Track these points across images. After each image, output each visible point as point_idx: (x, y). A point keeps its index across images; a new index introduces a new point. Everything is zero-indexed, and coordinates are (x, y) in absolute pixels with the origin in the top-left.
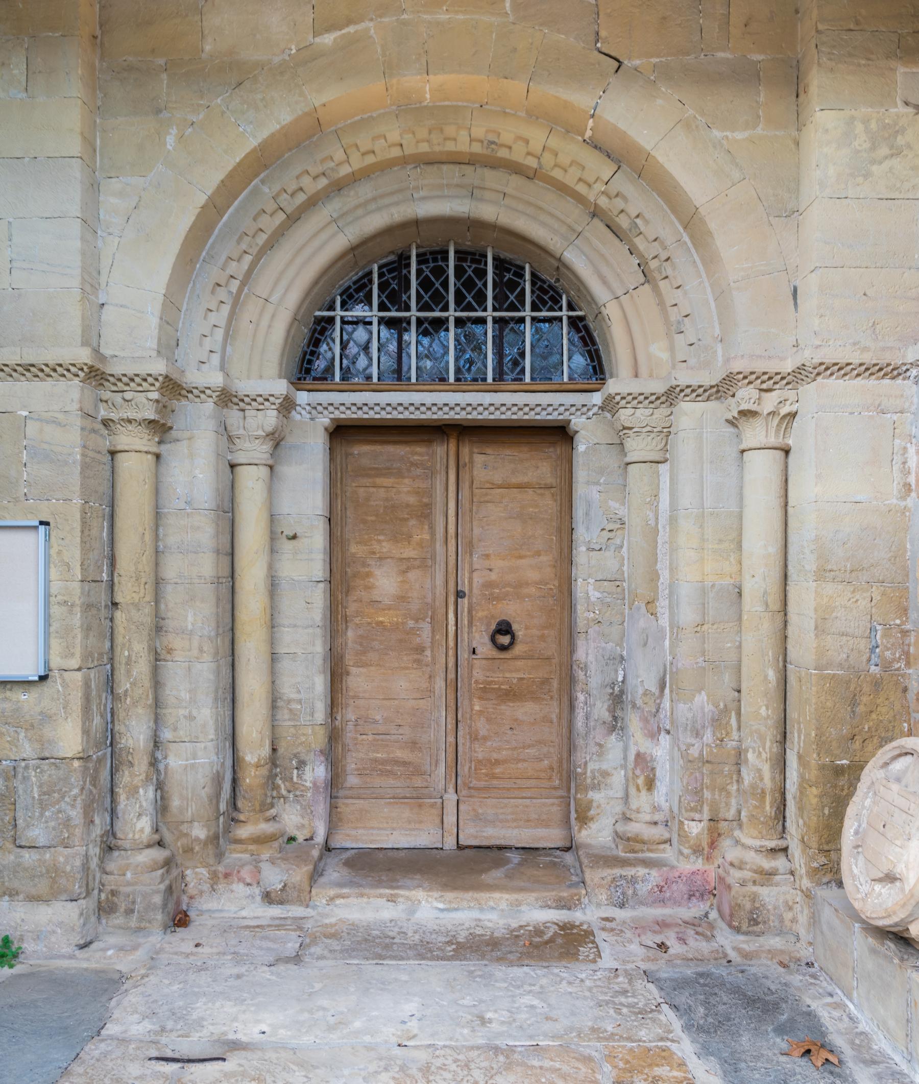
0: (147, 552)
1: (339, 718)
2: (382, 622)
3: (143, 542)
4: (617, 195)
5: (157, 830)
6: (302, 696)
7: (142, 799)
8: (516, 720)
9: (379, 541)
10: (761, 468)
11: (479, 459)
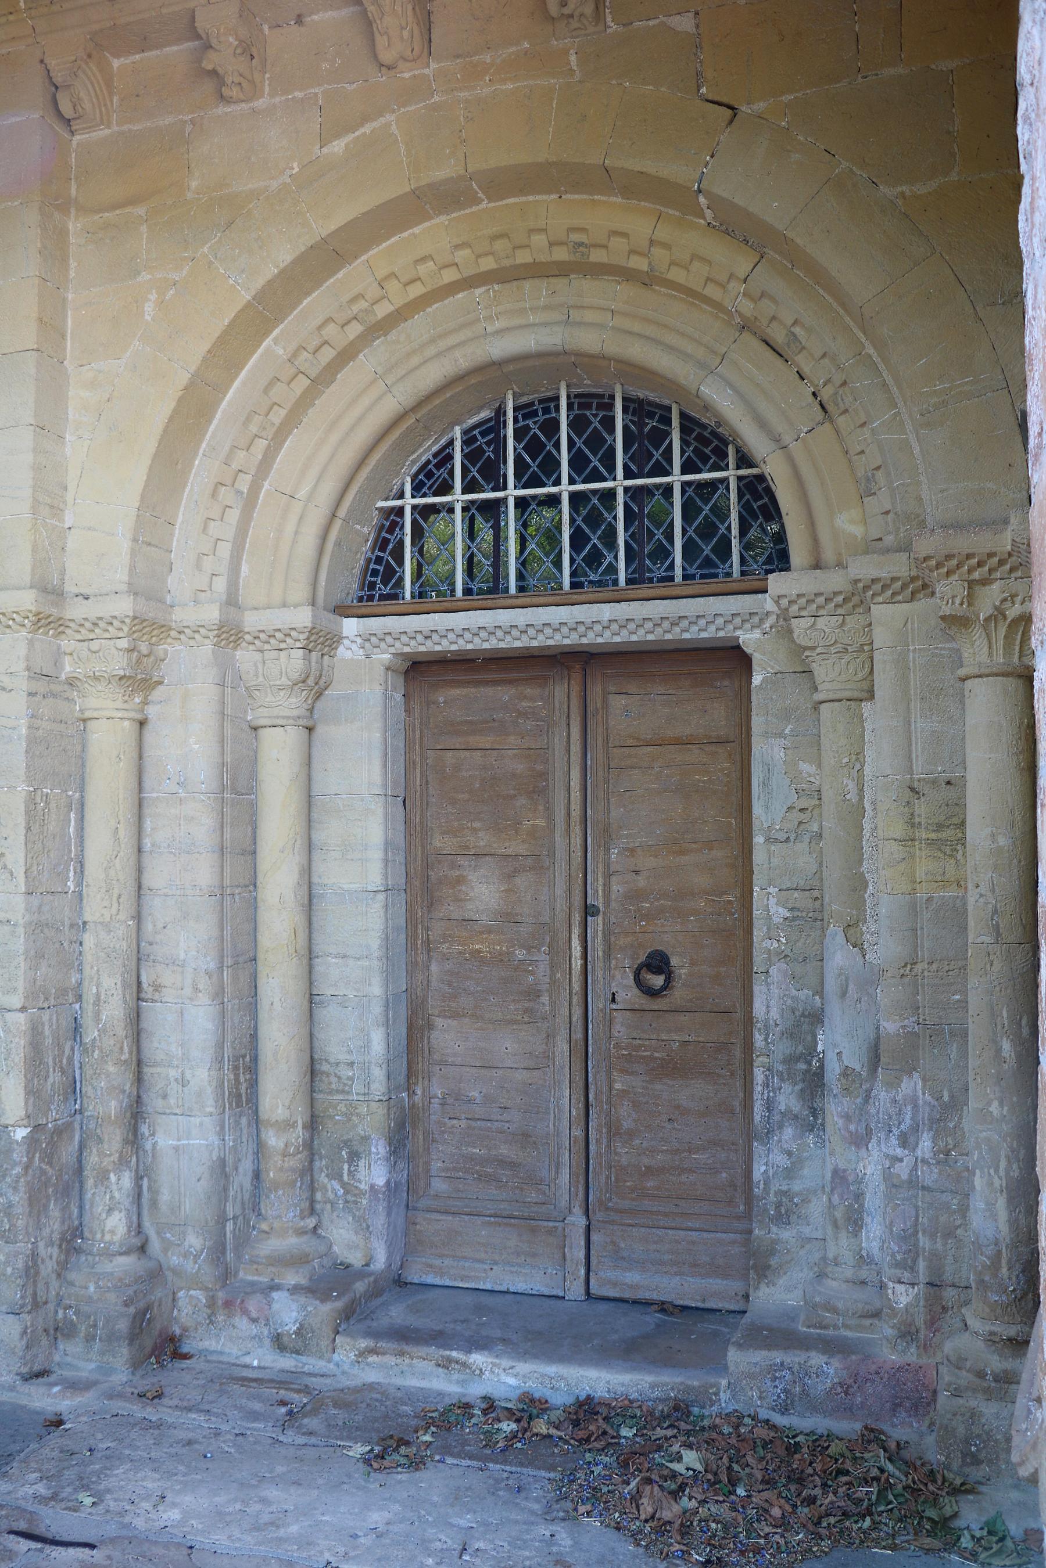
0: (122, 854)
1: (419, 1092)
2: (479, 951)
3: (117, 840)
4: (763, 295)
5: (139, 1232)
6: (354, 1058)
7: (114, 1187)
8: (678, 1107)
9: (475, 830)
10: (985, 704)
11: (617, 702)
